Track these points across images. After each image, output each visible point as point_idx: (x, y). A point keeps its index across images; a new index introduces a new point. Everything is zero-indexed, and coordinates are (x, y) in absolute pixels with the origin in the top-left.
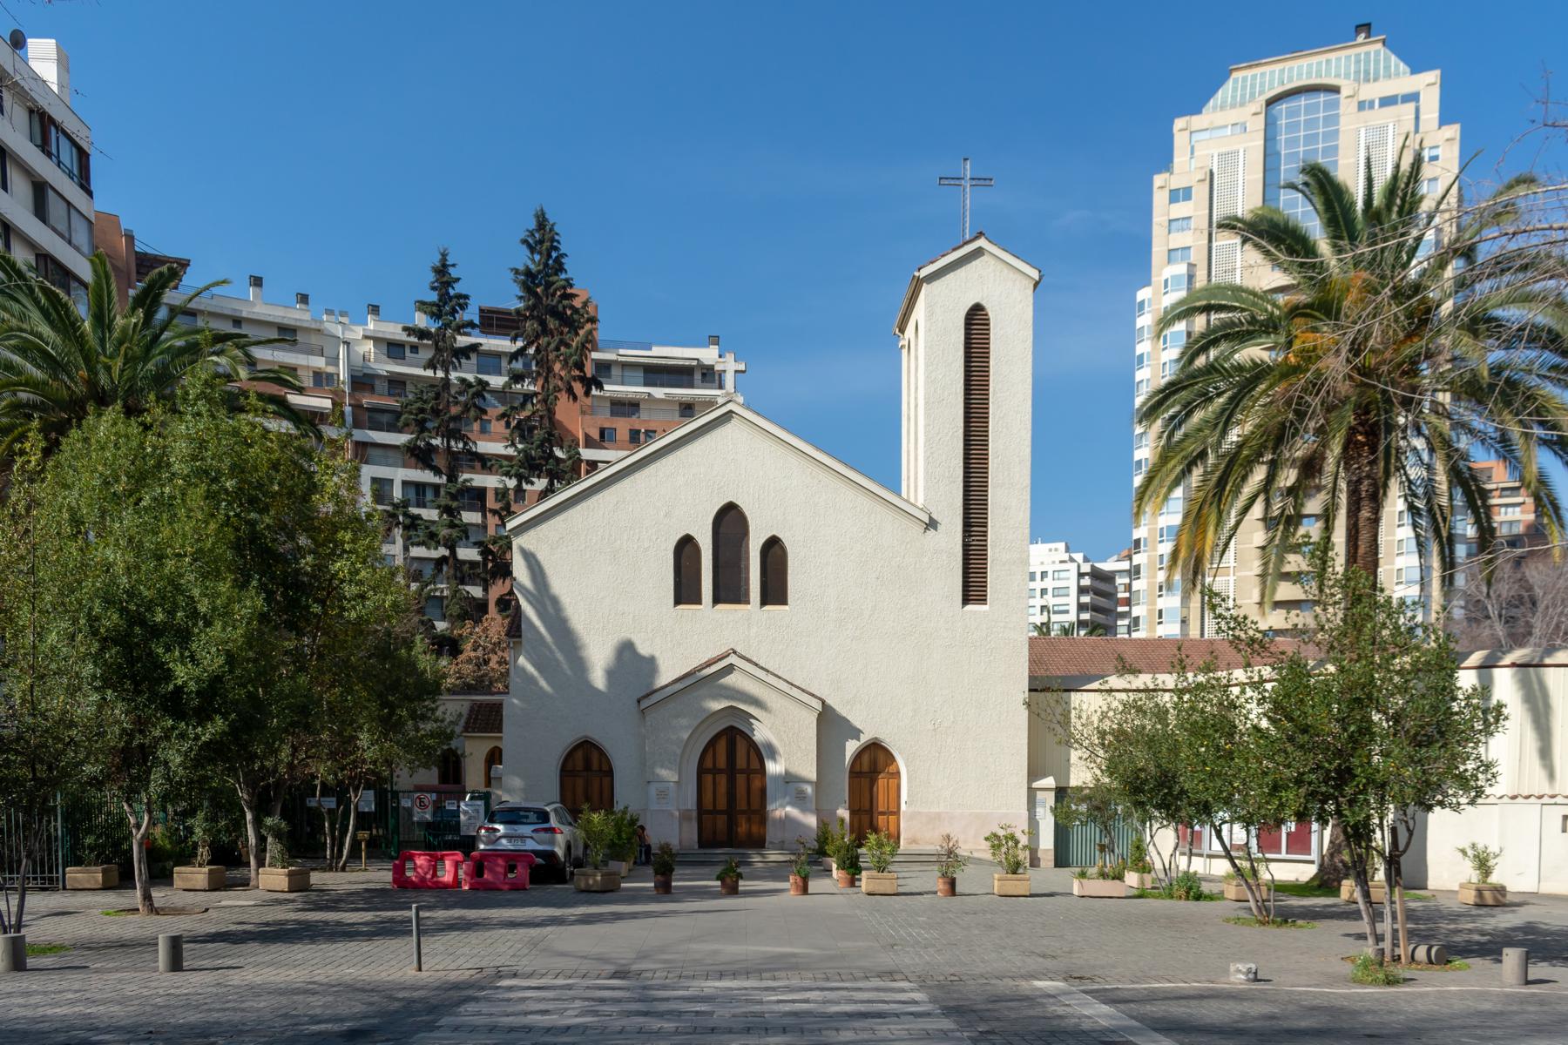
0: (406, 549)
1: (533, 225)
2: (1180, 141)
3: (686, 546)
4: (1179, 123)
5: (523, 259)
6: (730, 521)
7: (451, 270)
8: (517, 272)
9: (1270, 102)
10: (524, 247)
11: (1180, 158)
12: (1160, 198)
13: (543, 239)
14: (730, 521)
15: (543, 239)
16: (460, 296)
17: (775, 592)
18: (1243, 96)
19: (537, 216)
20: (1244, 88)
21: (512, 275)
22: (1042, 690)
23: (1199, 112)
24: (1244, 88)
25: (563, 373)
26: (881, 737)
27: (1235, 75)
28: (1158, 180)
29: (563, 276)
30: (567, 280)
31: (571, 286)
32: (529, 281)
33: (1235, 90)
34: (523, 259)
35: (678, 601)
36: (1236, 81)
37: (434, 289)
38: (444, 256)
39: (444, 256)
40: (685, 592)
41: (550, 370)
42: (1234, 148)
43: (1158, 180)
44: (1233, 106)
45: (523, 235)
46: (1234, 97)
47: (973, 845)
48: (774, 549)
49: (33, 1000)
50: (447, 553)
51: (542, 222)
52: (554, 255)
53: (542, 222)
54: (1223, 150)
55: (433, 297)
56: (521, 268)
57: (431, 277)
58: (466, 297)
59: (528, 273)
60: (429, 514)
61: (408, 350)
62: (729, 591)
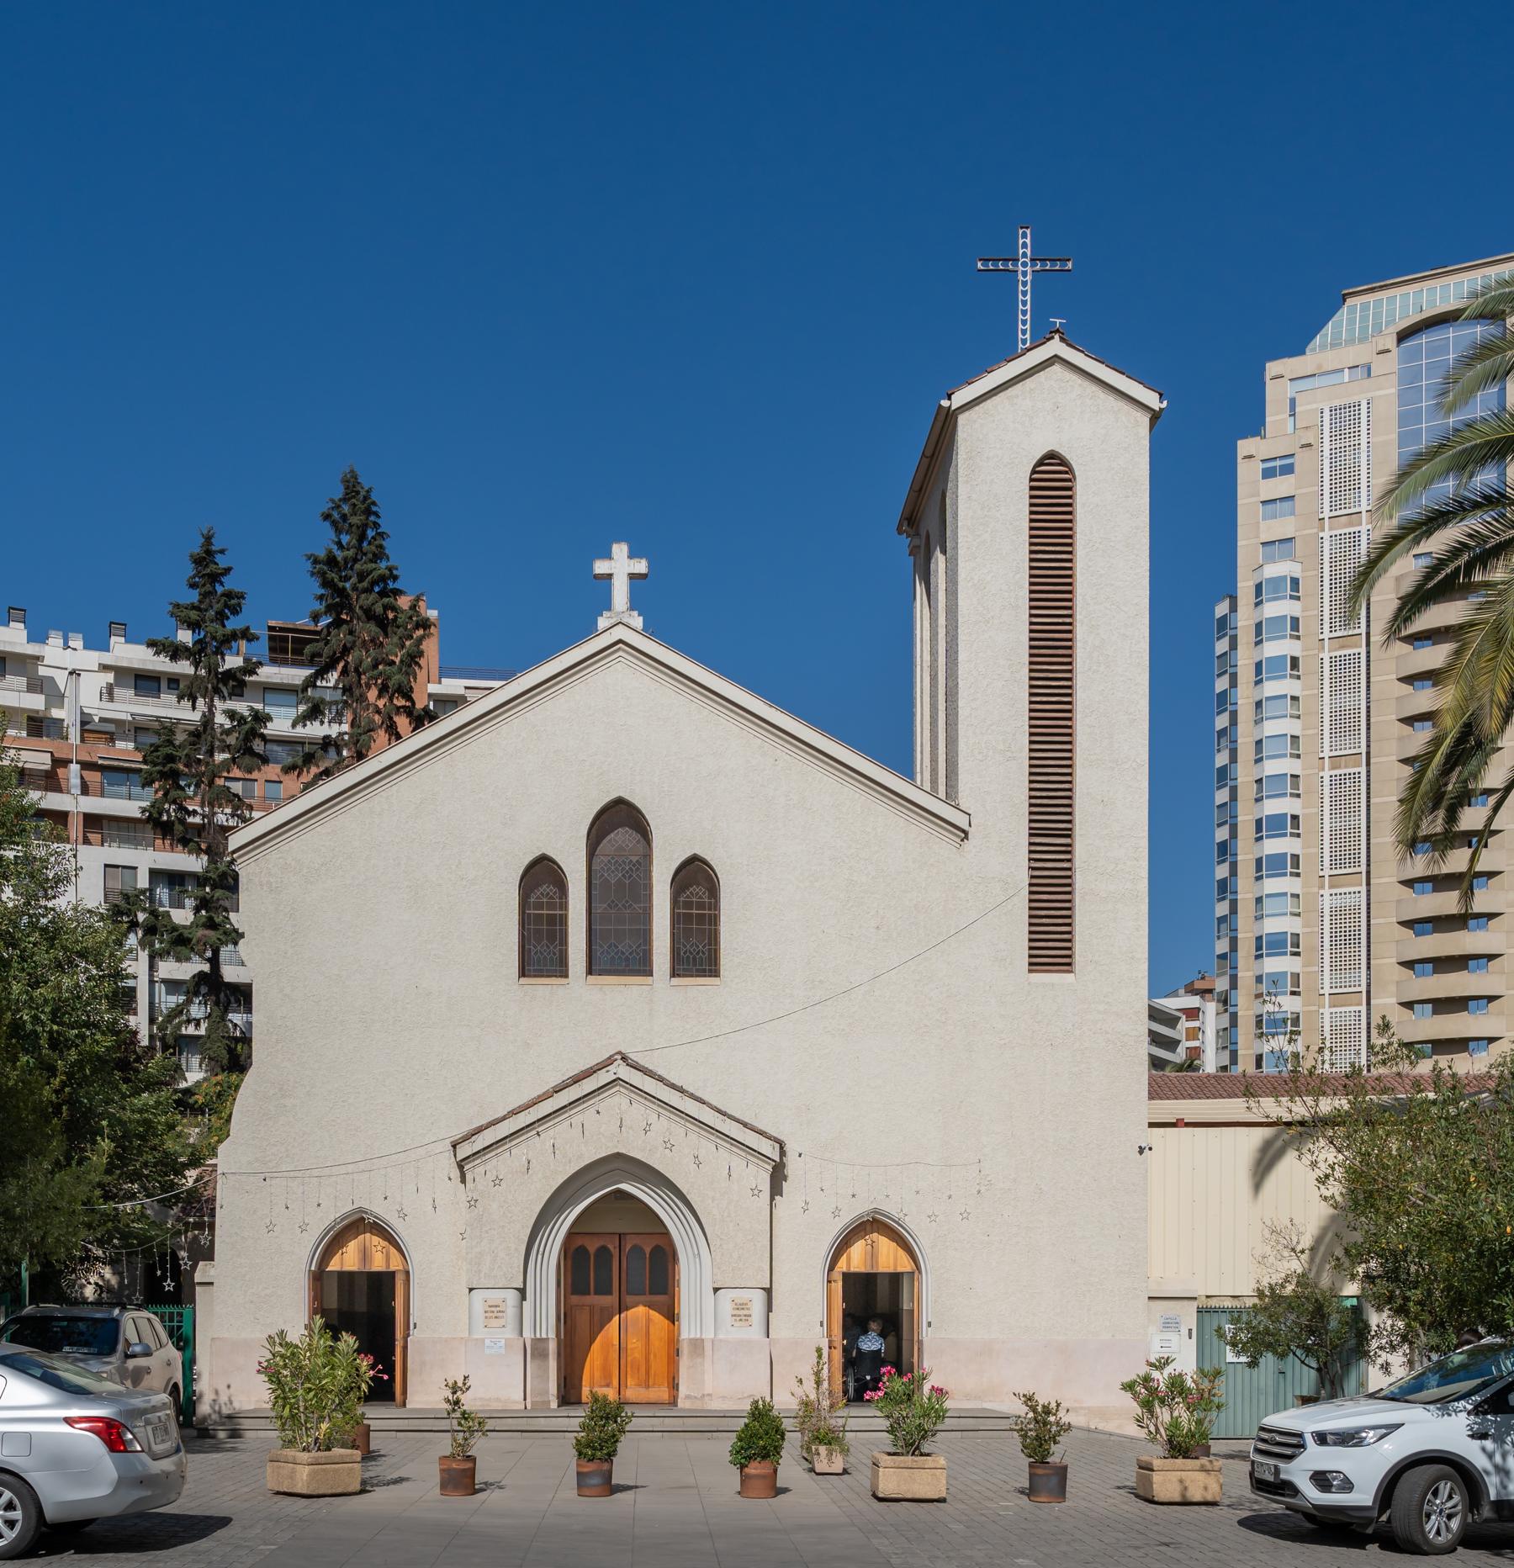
0: (152, 967)
1: (339, 492)
2: (1276, 394)
3: (541, 876)
4: (1273, 368)
5: (323, 540)
6: (619, 821)
7: (219, 558)
8: (316, 561)
9: (1403, 336)
10: (327, 524)
11: (1275, 416)
12: (1247, 474)
13: (356, 512)
14: (619, 821)
15: (356, 512)
16: (229, 595)
17: (698, 954)
18: (1363, 329)
19: (345, 481)
20: (1364, 319)
21: (309, 566)
22: (1173, 1125)
23: (1303, 353)
24: (1364, 319)
25: (381, 703)
26: (886, 1207)
27: (1350, 301)
28: (1245, 446)
29: (383, 564)
30: (390, 569)
31: (395, 578)
32: (328, 568)
33: (1351, 321)
34: (323, 540)
35: (526, 969)
36: (1352, 309)
37: (193, 586)
38: (208, 539)
39: (208, 539)
40: (540, 953)
41: (362, 698)
42: (1355, 399)
43: (1245, 446)
44: (1351, 341)
45: (326, 507)
46: (1351, 331)
47: (1098, 1405)
48: (696, 877)
49: (825, 1373)
50: (206, 967)
51: (352, 487)
52: (370, 533)
53: (352, 487)
54: (1336, 403)
55: (193, 596)
56: (322, 554)
57: (189, 570)
58: (241, 596)
59: (331, 561)
60: (183, 916)
61: (164, 684)
62: (619, 954)
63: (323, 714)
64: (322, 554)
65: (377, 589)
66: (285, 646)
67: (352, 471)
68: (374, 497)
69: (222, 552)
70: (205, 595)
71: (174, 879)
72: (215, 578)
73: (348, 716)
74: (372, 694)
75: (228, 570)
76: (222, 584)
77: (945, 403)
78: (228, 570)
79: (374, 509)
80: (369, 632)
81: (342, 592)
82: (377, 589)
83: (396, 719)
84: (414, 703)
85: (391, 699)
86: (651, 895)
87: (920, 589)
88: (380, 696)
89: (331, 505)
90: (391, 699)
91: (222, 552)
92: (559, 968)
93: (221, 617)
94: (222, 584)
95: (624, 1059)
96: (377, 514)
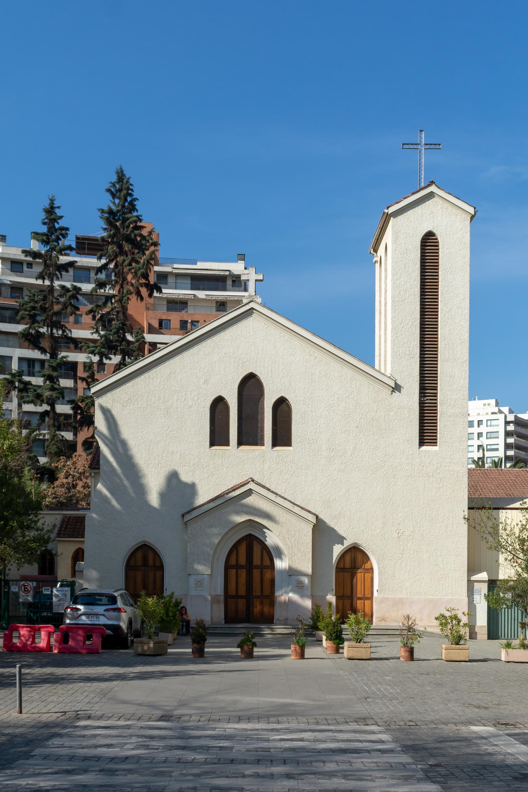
0: (20, 405)
3: (218, 405)
5: (107, 202)
6: (250, 386)
7: (57, 211)
8: (103, 211)
13: (122, 188)
14: (250, 386)
15: (122, 188)
16: (62, 229)
17: (282, 437)
19: (118, 173)
21: (99, 214)
25: (133, 281)
29: (135, 214)
30: (138, 217)
32: (111, 217)
34: (107, 202)
37: (44, 223)
38: (52, 201)
39: (52, 201)
40: (218, 437)
45: (108, 186)
47: (426, 623)
48: (282, 406)
51: (121, 177)
52: (129, 199)
53: (121, 177)
56: (106, 208)
57: (43, 215)
58: (67, 229)
60: (37, 381)
61: (25, 266)
62: (249, 436)
63: (106, 287)
64: (106, 208)
65: (132, 226)
66: (86, 245)
67: (121, 168)
68: (131, 181)
69: (59, 207)
70: (49, 229)
71: (31, 362)
72: (55, 220)
73: (118, 287)
74: (130, 277)
75: (61, 217)
76: (58, 223)
77: (386, 211)
78: (61, 217)
79: (131, 187)
80: (129, 248)
81: (116, 227)
82: (132, 226)
83: (140, 288)
84: (149, 282)
85: (138, 281)
86: (264, 412)
87: (265, 530)
88: (133, 278)
89: (110, 185)
90: (138, 281)
91: (59, 207)
92: (227, 443)
93: (58, 239)
94: (58, 223)
95: (253, 481)
96: (132, 190)
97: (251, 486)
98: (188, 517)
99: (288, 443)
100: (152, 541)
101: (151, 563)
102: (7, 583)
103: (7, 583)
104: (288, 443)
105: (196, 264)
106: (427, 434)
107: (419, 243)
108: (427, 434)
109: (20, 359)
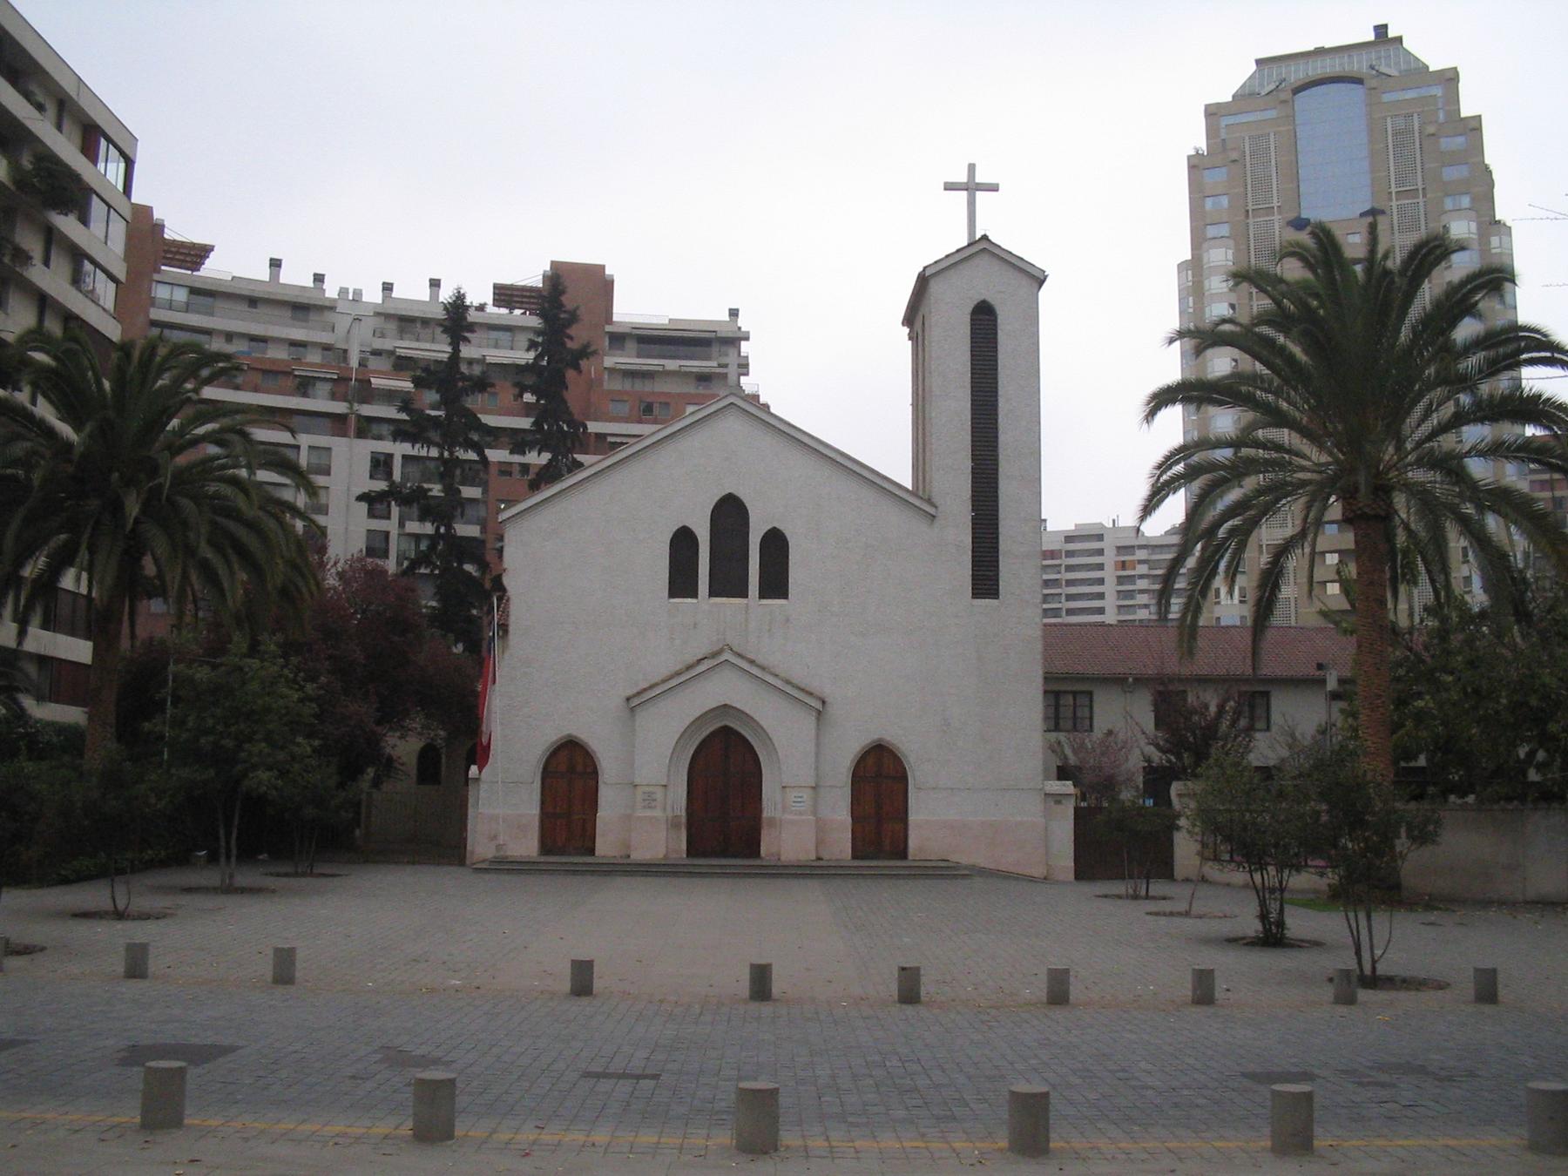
0: (401, 524)
3: (683, 541)
6: (730, 512)
14: (730, 512)
17: (776, 585)
40: (681, 583)
48: (776, 543)
62: (728, 583)
69: (435, 284)
97: (727, 656)
98: (635, 702)
99: (784, 594)
100: (584, 735)
101: (580, 768)
102: (1148, 878)
103: (1148, 878)
104: (784, 594)
105: (524, 453)
106: (985, 581)
107: (968, 318)
108: (985, 581)
109: (406, 458)
